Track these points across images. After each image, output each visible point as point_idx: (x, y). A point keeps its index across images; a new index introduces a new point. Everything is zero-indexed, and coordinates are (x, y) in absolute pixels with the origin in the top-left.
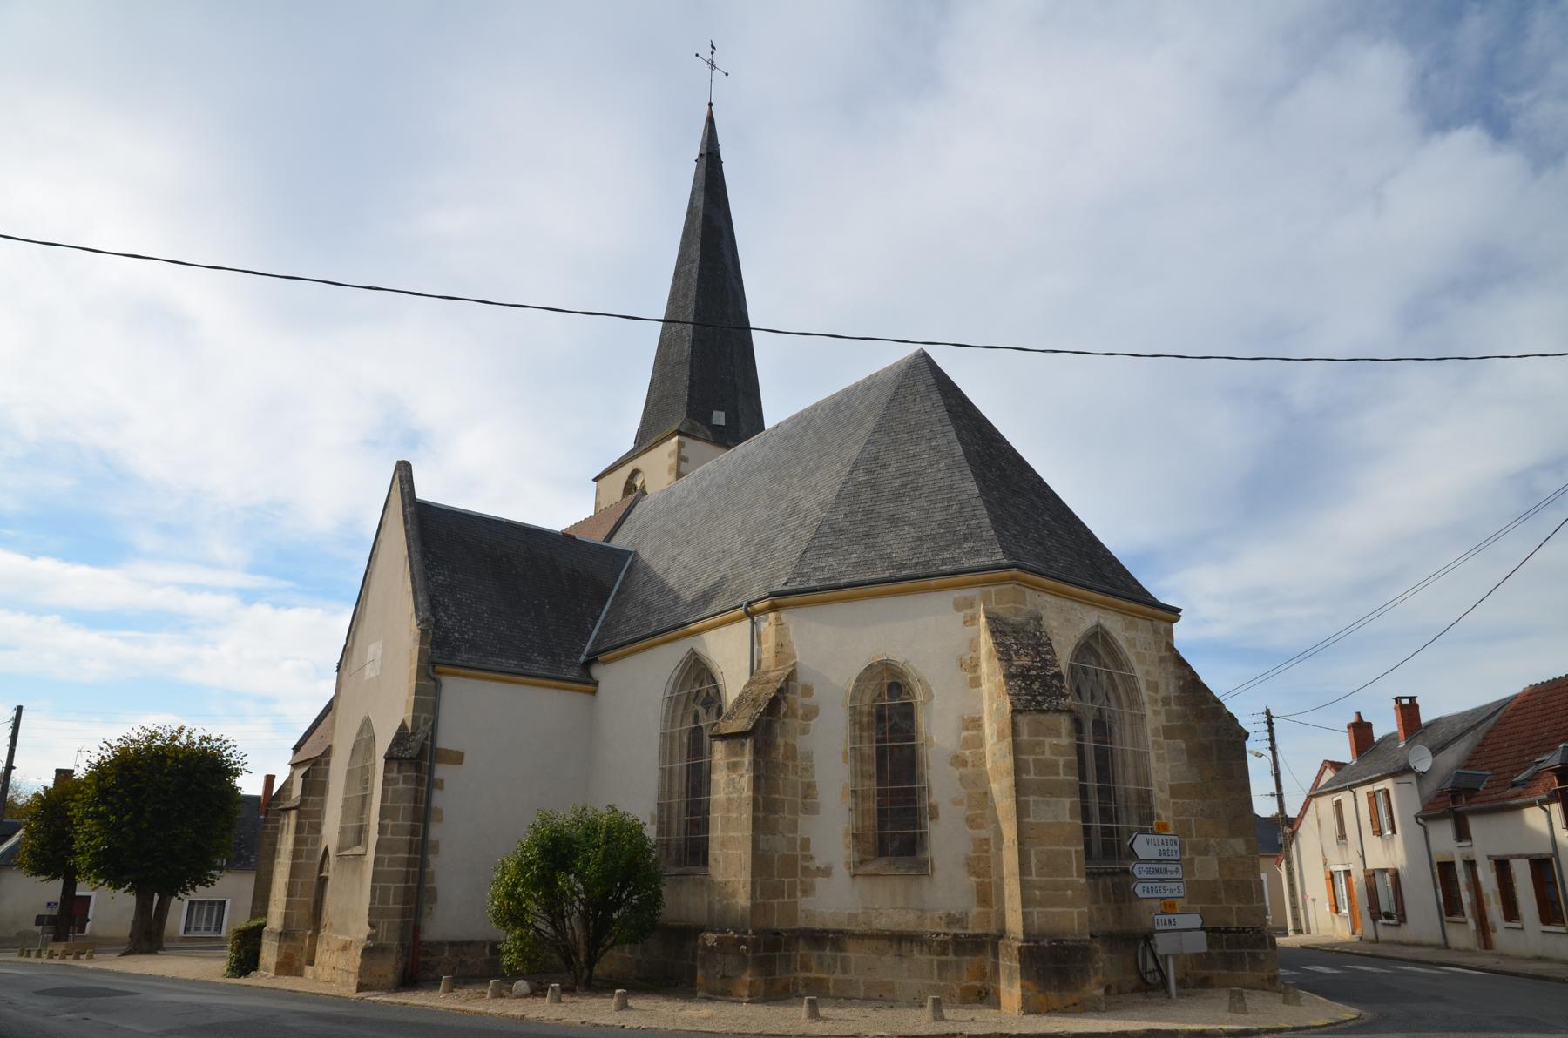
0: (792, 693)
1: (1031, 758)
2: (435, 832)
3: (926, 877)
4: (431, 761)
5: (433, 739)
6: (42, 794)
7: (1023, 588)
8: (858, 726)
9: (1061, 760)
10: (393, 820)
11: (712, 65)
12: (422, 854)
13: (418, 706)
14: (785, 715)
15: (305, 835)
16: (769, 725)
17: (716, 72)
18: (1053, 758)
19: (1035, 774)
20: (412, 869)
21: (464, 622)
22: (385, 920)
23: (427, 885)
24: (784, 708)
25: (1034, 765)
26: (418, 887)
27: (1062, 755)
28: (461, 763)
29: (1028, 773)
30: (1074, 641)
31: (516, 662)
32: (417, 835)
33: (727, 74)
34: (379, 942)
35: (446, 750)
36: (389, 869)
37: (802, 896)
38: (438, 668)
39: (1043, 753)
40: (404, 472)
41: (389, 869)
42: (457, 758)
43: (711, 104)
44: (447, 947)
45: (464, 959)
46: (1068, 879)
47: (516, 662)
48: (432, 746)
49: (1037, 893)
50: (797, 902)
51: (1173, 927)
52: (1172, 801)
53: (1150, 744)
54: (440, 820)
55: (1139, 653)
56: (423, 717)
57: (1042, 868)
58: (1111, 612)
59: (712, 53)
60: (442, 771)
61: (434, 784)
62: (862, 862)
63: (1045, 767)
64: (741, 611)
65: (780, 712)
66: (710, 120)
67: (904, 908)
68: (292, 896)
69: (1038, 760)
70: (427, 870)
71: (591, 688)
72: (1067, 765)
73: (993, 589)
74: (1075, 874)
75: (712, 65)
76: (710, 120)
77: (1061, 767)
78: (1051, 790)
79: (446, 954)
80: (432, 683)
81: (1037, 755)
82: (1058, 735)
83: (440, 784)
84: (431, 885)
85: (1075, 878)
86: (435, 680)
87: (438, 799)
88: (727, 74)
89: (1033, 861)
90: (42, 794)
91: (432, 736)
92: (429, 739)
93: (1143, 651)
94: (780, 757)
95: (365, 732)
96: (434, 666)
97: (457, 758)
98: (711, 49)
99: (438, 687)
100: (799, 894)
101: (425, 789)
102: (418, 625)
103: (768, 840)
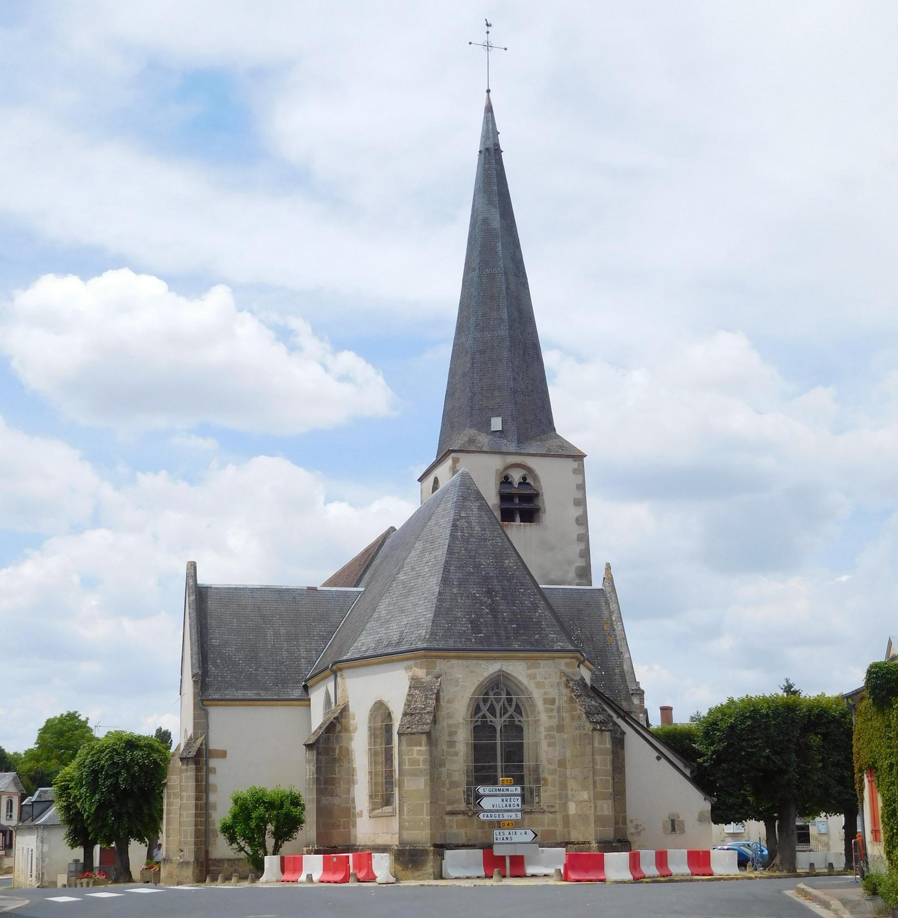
0: (346, 719)
1: (407, 758)
2: (213, 798)
3: (394, 817)
4: (206, 757)
5: (207, 744)
6: (162, 731)
7: (434, 660)
8: (373, 737)
9: (421, 758)
10: (186, 793)
11: (488, 46)
12: (206, 811)
13: (196, 726)
14: (339, 732)
15: (172, 800)
16: (328, 740)
17: (493, 51)
18: (418, 757)
19: (408, 766)
20: (199, 819)
21: (226, 669)
22: (188, 847)
23: (211, 828)
24: (338, 728)
25: (408, 761)
26: (206, 829)
27: (422, 756)
28: (225, 757)
29: (405, 765)
30: (477, 683)
31: (256, 692)
32: (201, 799)
33: (506, 49)
34: (185, 859)
35: (216, 750)
36: (187, 819)
37: (353, 828)
38: (205, 703)
39: (413, 755)
40: (192, 567)
41: (187, 819)
42: (223, 754)
43: (488, 91)
44: (226, 862)
45: (237, 868)
46: (422, 817)
47: (256, 692)
48: (206, 748)
49: (406, 824)
50: (350, 831)
51: (509, 841)
52: (558, 769)
53: (543, 736)
54: (216, 791)
55: (538, 682)
56: (200, 732)
57: (409, 812)
58: (514, 661)
59: (488, 33)
60: (213, 763)
61: (210, 770)
62: (373, 810)
63: (414, 762)
64: (328, 672)
65: (336, 730)
66: (489, 109)
67: (386, 833)
68: (168, 837)
69: (410, 759)
70: (210, 819)
71: (306, 703)
72: (424, 761)
73: (419, 661)
74: (425, 814)
75: (488, 46)
76: (489, 109)
77: (421, 762)
78: (415, 774)
79: (226, 866)
80: (203, 712)
81: (410, 756)
82: (421, 746)
83: (214, 771)
84: (213, 827)
85: (425, 817)
86: (204, 710)
87: (212, 779)
88: (506, 49)
89: (405, 809)
90: (162, 731)
91: (206, 742)
92: (204, 745)
93: (543, 680)
94: (336, 755)
95: (12, 797)
96: (202, 702)
97: (223, 754)
98: (486, 28)
99: (206, 715)
100: (351, 827)
101: (204, 773)
102: (192, 678)
103: (328, 799)
